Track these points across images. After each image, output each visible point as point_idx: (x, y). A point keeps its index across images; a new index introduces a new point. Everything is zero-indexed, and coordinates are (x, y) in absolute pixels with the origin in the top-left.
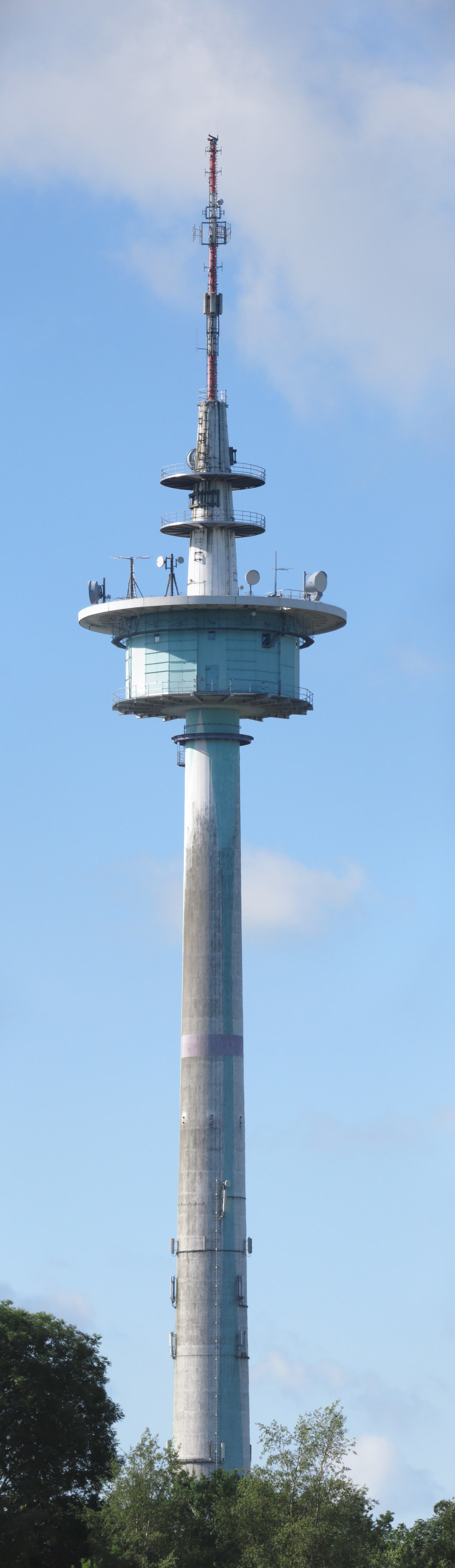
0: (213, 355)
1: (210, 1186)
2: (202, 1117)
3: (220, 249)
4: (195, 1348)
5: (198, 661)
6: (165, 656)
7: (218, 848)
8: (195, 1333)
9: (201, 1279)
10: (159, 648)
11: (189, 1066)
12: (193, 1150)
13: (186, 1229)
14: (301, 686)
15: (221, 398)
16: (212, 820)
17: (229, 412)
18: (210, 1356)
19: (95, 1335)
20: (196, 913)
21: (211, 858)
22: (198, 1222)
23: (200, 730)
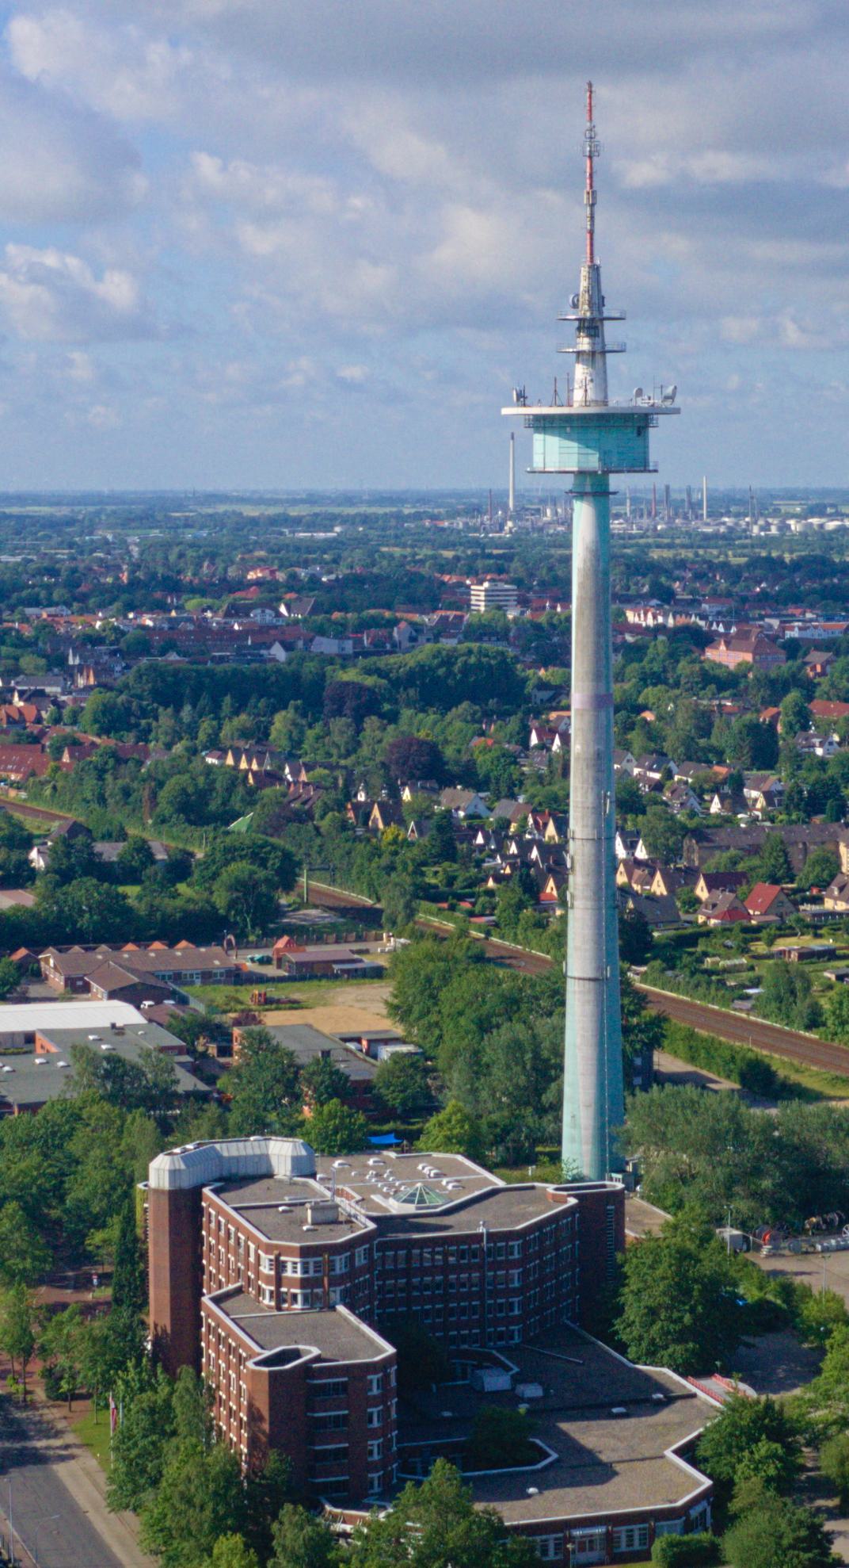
0: (591, 232)
1: (598, 797)
2: (591, 750)
3: (595, 159)
4: (589, 904)
5: (599, 449)
6: (575, 445)
7: (601, 568)
8: (589, 893)
9: (593, 858)
10: (569, 437)
11: (582, 715)
12: (586, 771)
13: (571, 889)
14: (569, 974)
15: (597, 262)
16: (597, 550)
17: (602, 271)
18: (599, 909)
19: (656, 464)
20: (587, 612)
21: (597, 576)
22: (590, 821)
23: (588, 489)
